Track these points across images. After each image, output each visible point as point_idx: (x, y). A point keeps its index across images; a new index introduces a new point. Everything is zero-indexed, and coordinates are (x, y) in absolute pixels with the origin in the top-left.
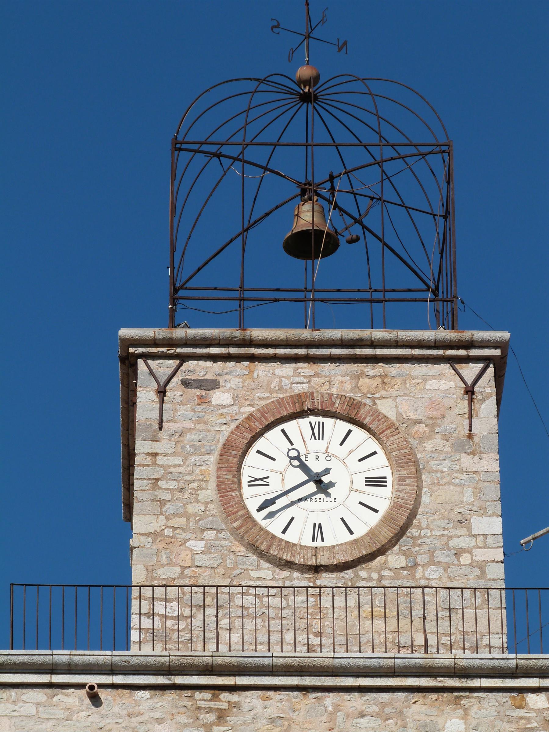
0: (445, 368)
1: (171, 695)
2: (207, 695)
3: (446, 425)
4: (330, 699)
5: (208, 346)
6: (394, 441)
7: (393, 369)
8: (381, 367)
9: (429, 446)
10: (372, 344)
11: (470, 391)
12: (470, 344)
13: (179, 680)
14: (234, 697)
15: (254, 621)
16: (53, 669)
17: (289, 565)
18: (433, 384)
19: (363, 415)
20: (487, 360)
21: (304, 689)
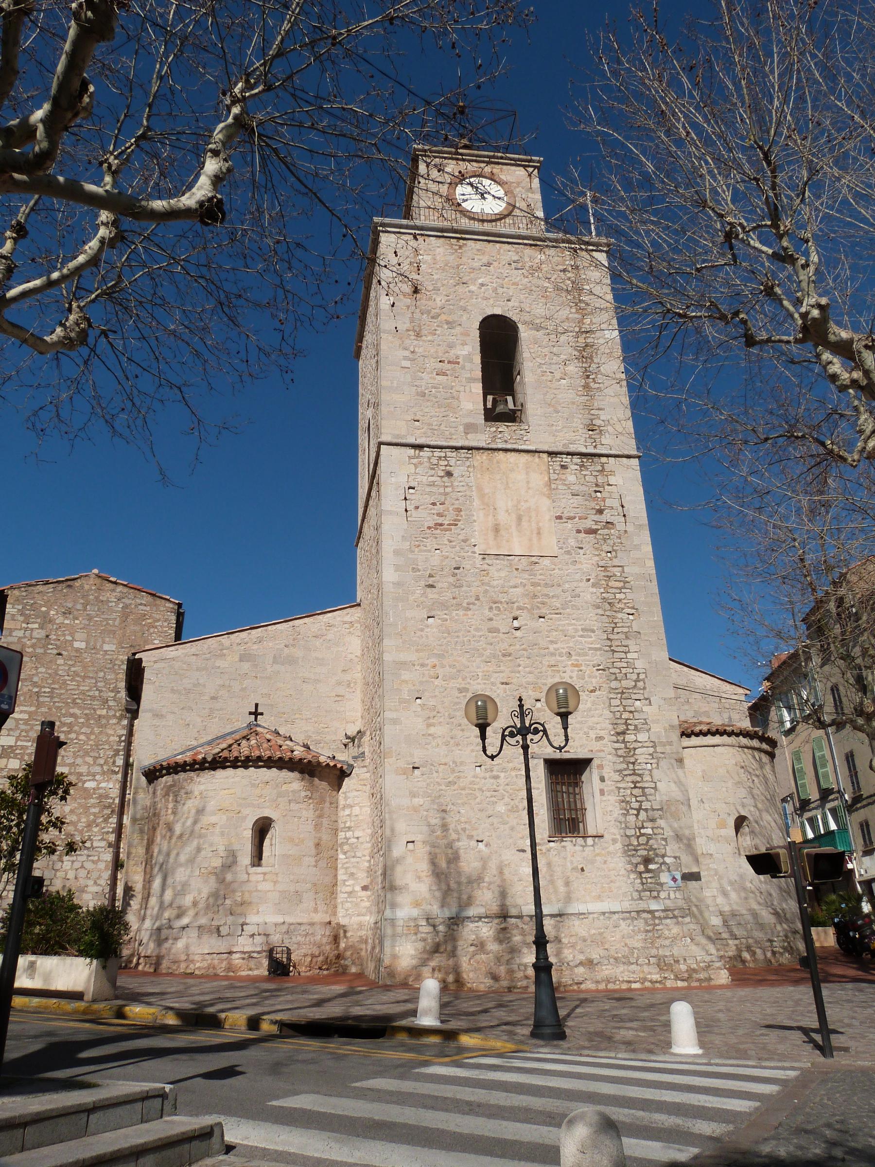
0: (522, 168)
1: (443, 239)
2: (455, 240)
3: (523, 185)
4: (498, 245)
5: (400, 228)
6: (506, 186)
7: (505, 167)
8: (500, 166)
9: (518, 190)
10: (498, 158)
11: (530, 175)
12: (530, 161)
13: (445, 234)
14: (465, 242)
15: (114, 820)
16: (401, 226)
17: (474, 219)
18: (517, 173)
19: (495, 178)
20: (535, 167)
21: (489, 241)
